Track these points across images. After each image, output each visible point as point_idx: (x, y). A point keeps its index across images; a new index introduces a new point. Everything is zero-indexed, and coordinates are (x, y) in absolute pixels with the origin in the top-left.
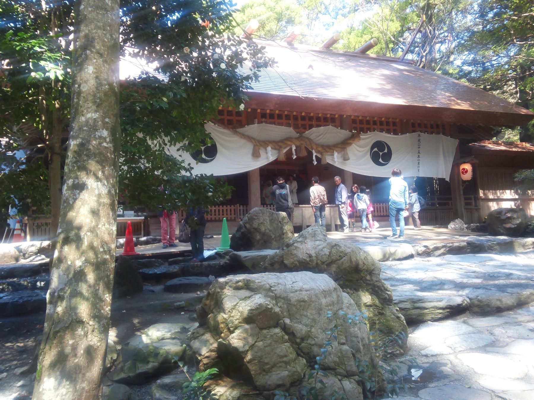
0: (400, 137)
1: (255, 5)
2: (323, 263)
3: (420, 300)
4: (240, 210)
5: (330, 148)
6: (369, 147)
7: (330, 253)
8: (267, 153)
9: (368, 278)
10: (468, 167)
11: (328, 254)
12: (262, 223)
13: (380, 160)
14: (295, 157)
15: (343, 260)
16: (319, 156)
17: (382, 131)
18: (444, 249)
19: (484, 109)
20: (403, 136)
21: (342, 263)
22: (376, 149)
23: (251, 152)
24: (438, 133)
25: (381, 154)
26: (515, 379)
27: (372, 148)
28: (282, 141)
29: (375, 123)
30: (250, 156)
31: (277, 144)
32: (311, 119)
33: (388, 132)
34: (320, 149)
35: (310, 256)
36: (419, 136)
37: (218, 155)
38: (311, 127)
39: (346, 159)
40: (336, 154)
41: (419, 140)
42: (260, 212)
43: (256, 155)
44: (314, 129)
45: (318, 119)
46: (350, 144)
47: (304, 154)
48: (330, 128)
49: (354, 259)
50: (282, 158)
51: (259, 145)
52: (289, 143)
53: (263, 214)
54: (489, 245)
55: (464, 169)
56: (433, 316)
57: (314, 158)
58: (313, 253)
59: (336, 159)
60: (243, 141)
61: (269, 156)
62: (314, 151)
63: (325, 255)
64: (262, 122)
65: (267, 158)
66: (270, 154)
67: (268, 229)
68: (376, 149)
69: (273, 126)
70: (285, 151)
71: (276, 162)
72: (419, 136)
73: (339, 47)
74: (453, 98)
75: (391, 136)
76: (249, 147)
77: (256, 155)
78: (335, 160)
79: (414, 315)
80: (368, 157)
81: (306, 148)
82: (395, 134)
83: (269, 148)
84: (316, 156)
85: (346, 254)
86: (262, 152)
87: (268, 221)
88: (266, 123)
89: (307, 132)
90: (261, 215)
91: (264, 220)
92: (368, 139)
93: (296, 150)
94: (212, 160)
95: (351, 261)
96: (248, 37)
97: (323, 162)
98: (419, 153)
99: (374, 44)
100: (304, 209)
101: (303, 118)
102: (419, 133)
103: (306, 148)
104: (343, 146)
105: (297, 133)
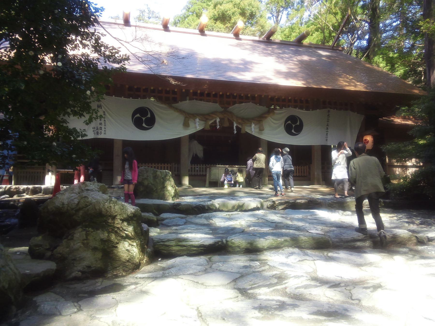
0: (311, 112)
1: (225, 2)
2: (72, 209)
3: (185, 240)
4: (175, 167)
5: (248, 120)
6: (284, 120)
7: (79, 203)
8: (195, 123)
9: (110, 221)
10: (369, 138)
11: (77, 203)
12: (146, 179)
13: (293, 131)
14: (218, 127)
15: (88, 207)
16: (240, 126)
17: (295, 107)
18: (287, 204)
19: (373, 91)
20: (314, 111)
21: (88, 210)
22: (289, 122)
23: (182, 123)
24: (346, 109)
25: (294, 126)
26: (227, 299)
27: (286, 121)
28: (208, 115)
29: (290, 101)
30: (181, 126)
31: (204, 117)
32: (235, 97)
33: (301, 108)
34: (240, 121)
35: (63, 204)
36: (329, 111)
37: (156, 125)
38: (234, 103)
39: (261, 130)
40: (253, 126)
41: (328, 115)
42: (145, 170)
43: (186, 125)
44: (237, 105)
45: (240, 97)
46: (266, 118)
47: (226, 124)
48: (251, 105)
49: (97, 208)
50: (208, 128)
51: (188, 117)
52: (214, 116)
53: (147, 172)
54: (330, 203)
55: (366, 140)
56: (188, 252)
57: (235, 128)
58: (66, 202)
59: (253, 130)
60: (176, 114)
61: (197, 126)
62: (235, 123)
63: (74, 203)
64: (193, 99)
65: (196, 127)
66: (197, 124)
67: (151, 183)
68: (289, 122)
69: (203, 102)
70: (210, 122)
71: (203, 131)
72: (329, 111)
73: (277, 37)
74: (354, 81)
75: (304, 111)
76: (181, 118)
77: (186, 125)
78: (253, 130)
79: (174, 250)
80: (282, 128)
81: (228, 119)
82: (306, 110)
83: (197, 120)
84: (237, 127)
85: (91, 204)
86: (191, 123)
87: (152, 177)
88: (196, 99)
89: (230, 107)
90: (145, 172)
91: (148, 176)
92: (282, 114)
93: (220, 122)
94: (150, 128)
95: (96, 209)
96: (363, 14)
97: (243, 132)
98: (328, 125)
99: (306, 35)
100: (220, 168)
101: (228, 97)
102: (329, 109)
103: (228, 119)
104: (259, 119)
105: (222, 108)
